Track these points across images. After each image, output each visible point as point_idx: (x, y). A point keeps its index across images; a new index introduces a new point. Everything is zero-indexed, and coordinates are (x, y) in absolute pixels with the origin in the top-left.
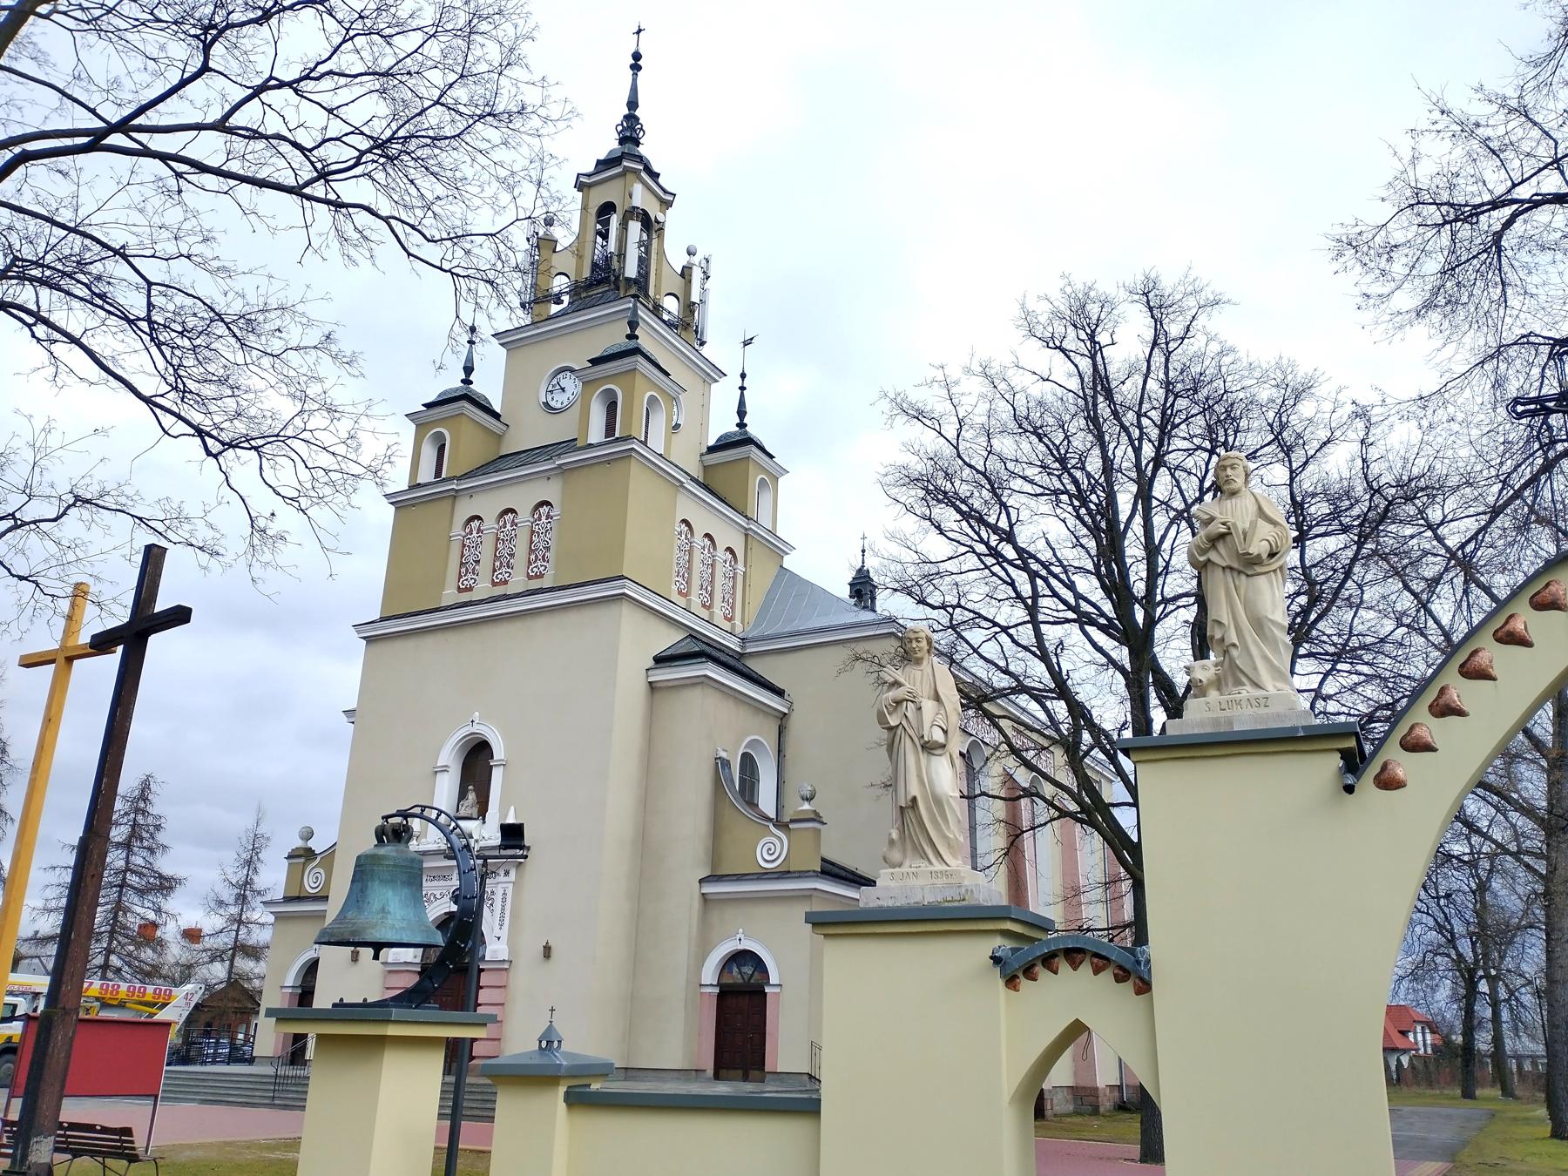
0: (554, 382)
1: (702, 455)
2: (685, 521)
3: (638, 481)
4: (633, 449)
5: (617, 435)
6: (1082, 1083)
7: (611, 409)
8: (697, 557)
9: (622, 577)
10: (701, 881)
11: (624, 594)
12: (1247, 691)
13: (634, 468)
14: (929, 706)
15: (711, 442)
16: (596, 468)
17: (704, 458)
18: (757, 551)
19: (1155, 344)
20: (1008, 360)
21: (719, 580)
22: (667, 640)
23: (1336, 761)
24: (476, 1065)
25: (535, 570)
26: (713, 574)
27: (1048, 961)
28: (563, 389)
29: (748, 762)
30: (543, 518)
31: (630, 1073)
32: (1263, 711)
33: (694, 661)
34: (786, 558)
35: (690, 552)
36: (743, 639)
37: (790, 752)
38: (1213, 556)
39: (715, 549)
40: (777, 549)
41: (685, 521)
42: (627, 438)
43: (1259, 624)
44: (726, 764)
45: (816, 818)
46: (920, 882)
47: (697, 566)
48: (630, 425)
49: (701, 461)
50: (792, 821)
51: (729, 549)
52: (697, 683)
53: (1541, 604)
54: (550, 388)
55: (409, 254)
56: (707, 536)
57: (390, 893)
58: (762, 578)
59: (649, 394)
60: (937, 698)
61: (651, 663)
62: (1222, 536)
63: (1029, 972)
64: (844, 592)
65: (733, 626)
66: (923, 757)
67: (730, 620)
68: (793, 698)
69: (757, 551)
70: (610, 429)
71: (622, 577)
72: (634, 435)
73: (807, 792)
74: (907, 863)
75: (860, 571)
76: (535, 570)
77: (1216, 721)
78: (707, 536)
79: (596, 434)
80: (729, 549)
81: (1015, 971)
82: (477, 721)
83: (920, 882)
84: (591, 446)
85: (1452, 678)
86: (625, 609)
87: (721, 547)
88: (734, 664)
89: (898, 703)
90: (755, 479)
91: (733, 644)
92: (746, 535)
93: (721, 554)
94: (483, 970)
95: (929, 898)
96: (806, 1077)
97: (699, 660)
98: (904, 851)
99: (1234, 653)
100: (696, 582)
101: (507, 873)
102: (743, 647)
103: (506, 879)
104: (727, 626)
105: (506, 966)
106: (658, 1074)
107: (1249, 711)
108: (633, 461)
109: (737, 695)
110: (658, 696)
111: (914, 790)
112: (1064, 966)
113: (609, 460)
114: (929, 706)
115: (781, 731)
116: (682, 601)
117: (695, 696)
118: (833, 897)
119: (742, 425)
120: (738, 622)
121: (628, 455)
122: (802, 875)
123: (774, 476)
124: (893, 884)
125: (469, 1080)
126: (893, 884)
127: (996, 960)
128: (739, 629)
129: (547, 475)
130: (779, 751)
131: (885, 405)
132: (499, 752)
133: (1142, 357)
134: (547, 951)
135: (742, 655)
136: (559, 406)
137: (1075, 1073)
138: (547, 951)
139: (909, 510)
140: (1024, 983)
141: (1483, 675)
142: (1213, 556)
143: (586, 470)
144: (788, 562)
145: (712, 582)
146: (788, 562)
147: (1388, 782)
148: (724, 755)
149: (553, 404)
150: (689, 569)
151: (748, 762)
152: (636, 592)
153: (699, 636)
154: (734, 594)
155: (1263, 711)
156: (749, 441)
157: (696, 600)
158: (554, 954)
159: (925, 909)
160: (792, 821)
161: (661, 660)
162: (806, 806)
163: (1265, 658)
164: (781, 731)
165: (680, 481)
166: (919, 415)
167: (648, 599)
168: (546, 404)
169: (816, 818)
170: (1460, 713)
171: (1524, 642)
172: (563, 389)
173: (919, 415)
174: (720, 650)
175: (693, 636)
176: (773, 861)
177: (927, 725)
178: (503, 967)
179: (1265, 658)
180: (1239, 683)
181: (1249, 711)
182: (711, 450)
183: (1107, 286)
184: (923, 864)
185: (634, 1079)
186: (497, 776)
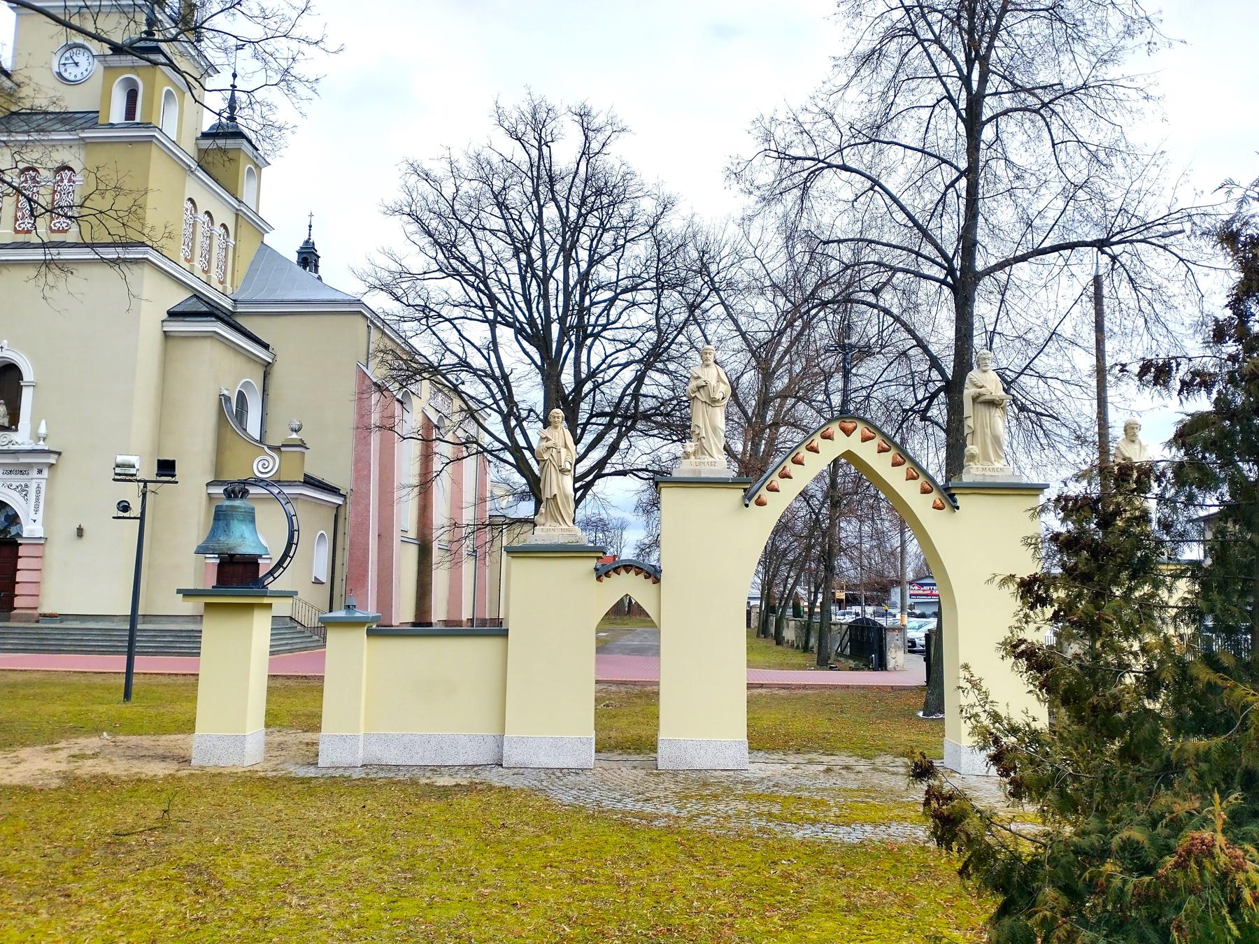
0: (67, 55)
1: (197, 139)
2: (191, 200)
3: (157, 161)
4: (154, 136)
5: (138, 120)
6: (452, 619)
7: (132, 96)
8: (199, 230)
9: (143, 244)
10: (208, 485)
11: (147, 259)
12: (707, 459)
13: (155, 152)
14: (563, 451)
15: (205, 129)
16: (117, 146)
17: (199, 142)
18: (245, 230)
19: (584, 153)
20: (485, 142)
21: (215, 250)
22: (177, 298)
23: (741, 493)
24: (18, 614)
25: (58, 225)
26: (210, 245)
27: (616, 570)
28: (76, 64)
29: (241, 396)
30: (66, 181)
31: (146, 618)
32: (713, 468)
33: (205, 319)
34: (266, 235)
35: (194, 225)
36: (235, 301)
37: (272, 392)
38: (698, 394)
39: (212, 224)
40: (260, 228)
41: (191, 200)
42: (146, 125)
43: (715, 429)
44: (228, 399)
45: (302, 445)
46: (557, 533)
47: (199, 238)
48: (151, 113)
49: (196, 144)
50: (284, 446)
51: (224, 226)
52: (208, 337)
53: (824, 437)
54: (63, 61)
55: (196, 101)
56: (208, 213)
57: (244, 527)
58: (248, 250)
59: (166, 89)
60: (566, 446)
61: (165, 316)
62: (703, 387)
63: (607, 575)
64: (294, 258)
65: (225, 288)
66: (560, 475)
67: (221, 283)
68: (276, 351)
69: (245, 230)
70: (130, 112)
71: (143, 244)
72: (154, 123)
73: (295, 425)
74: (548, 524)
75: (307, 242)
76: (58, 225)
77: (694, 471)
78: (208, 213)
79: (117, 114)
80: (224, 226)
81: (602, 574)
82: (6, 347)
83: (557, 533)
84: (112, 126)
85: (788, 463)
86: (147, 271)
87: (201, 209)
88: (227, 319)
89: (548, 448)
90: (246, 166)
91: (227, 304)
92: (237, 215)
93: (218, 230)
94: (21, 544)
95: (561, 541)
96: (288, 619)
97: (209, 319)
98: (546, 518)
99: (703, 441)
100: (198, 251)
101: (40, 472)
102: (234, 307)
103: (39, 476)
104: (220, 288)
105: (42, 542)
106: (172, 618)
107: (707, 467)
108: (153, 147)
109: (236, 347)
110: (171, 343)
111: (555, 491)
112: (623, 572)
113: (131, 142)
114: (563, 451)
115: (266, 376)
116: (187, 266)
117: (207, 347)
118: (310, 499)
119: (232, 118)
120: (228, 285)
121: (149, 140)
122: (290, 484)
123: (258, 165)
124: (543, 534)
125: (139, 627)
126: (543, 534)
127: (596, 569)
128: (229, 292)
129: (69, 144)
130: (264, 391)
131: (404, 166)
132: (28, 375)
133: (574, 160)
134: (80, 532)
135: (233, 313)
136: (72, 78)
137: (448, 612)
138: (80, 532)
139: (422, 250)
140: (605, 579)
141: (800, 463)
142: (698, 394)
143: (108, 146)
144: (268, 239)
145: (210, 251)
146: (268, 239)
147: (760, 503)
148: (226, 393)
149: (66, 75)
150: (193, 240)
151: (241, 396)
152: (155, 258)
153: (201, 296)
154: (226, 262)
155: (713, 468)
156: (240, 135)
157: (198, 265)
158: (86, 533)
159: (561, 545)
160: (284, 446)
161: (173, 315)
162: (294, 436)
163: (716, 444)
164: (266, 376)
165: (189, 166)
166: (427, 177)
167: (165, 264)
168: (59, 74)
169: (302, 445)
170: (790, 477)
171: (816, 451)
172: (76, 64)
173: (427, 177)
174: (216, 308)
175: (197, 296)
176: (266, 473)
177: (563, 461)
178: (40, 543)
179: (716, 444)
180: (703, 454)
181: (707, 467)
182: (205, 136)
183: (552, 100)
184: (554, 524)
185: (150, 622)
186: (27, 396)
